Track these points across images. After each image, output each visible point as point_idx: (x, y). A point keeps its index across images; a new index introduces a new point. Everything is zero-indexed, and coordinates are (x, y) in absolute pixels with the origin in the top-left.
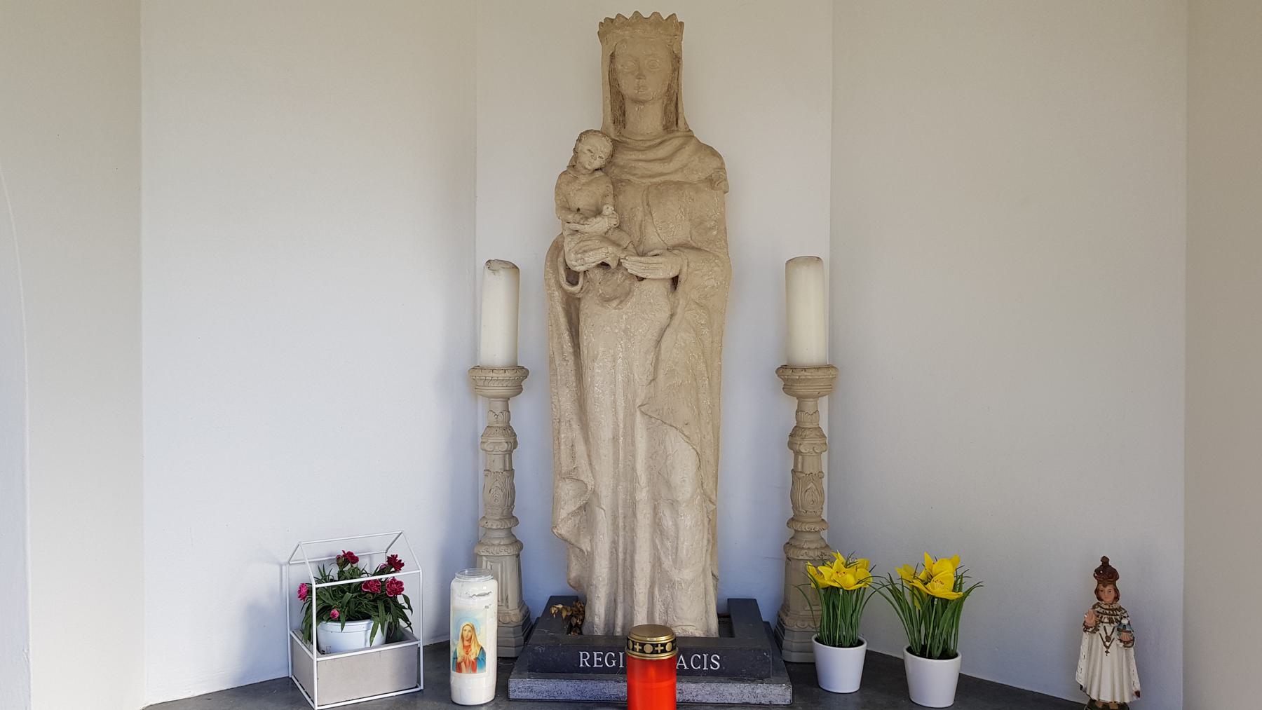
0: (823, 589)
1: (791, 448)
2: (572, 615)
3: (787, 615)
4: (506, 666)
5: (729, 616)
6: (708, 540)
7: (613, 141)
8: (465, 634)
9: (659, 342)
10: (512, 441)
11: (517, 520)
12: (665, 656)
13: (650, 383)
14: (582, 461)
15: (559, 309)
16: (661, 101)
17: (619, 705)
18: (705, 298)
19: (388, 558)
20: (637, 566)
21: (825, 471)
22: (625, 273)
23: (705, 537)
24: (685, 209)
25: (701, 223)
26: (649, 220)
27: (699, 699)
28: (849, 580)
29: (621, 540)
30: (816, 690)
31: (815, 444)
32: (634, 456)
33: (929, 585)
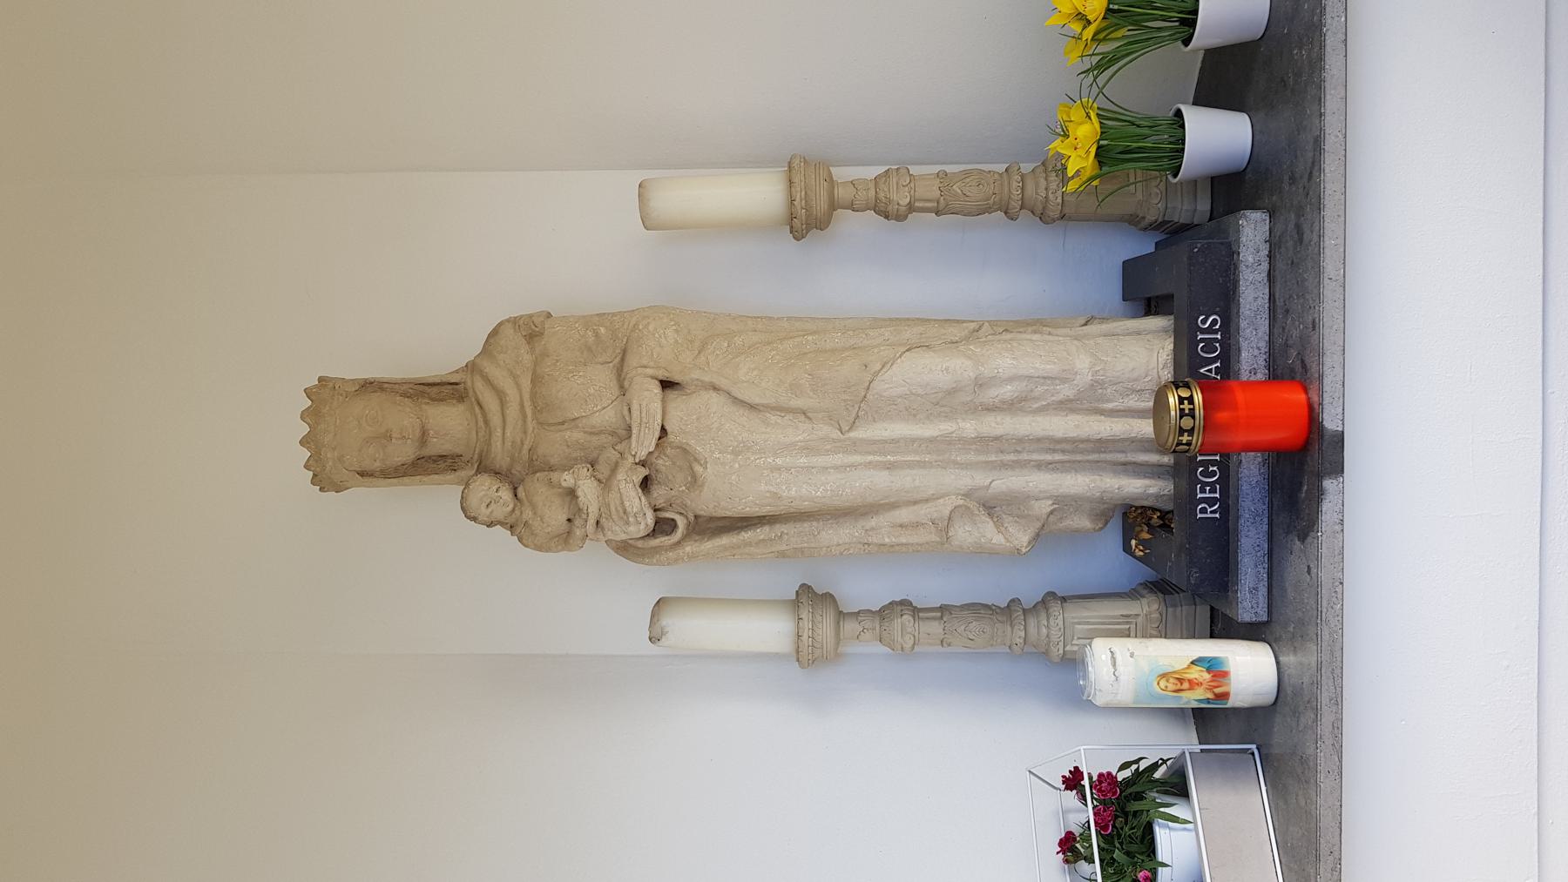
0: (1101, 170)
1: (906, 217)
2: (1148, 525)
3: (1144, 218)
4: (1222, 627)
5: (1149, 300)
6: (1035, 332)
7: (478, 472)
8: (1171, 687)
9: (752, 407)
10: (899, 608)
11: (1013, 601)
12: (1198, 398)
13: (810, 419)
14: (923, 512)
15: (710, 545)
16: (423, 406)
17: (1275, 461)
18: (691, 342)
19: (1066, 788)
20: (1072, 434)
21: (936, 169)
22: (656, 454)
23: (1029, 337)
24: (571, 372)
25: (589, 349)
26: (584, 421)
27: (1263, 345)
28: (1086, 131)
29: (1035, 457)
30: (1249, 176)
31: (897, 184)
32: (913, 440)
33: (1090, 18)
